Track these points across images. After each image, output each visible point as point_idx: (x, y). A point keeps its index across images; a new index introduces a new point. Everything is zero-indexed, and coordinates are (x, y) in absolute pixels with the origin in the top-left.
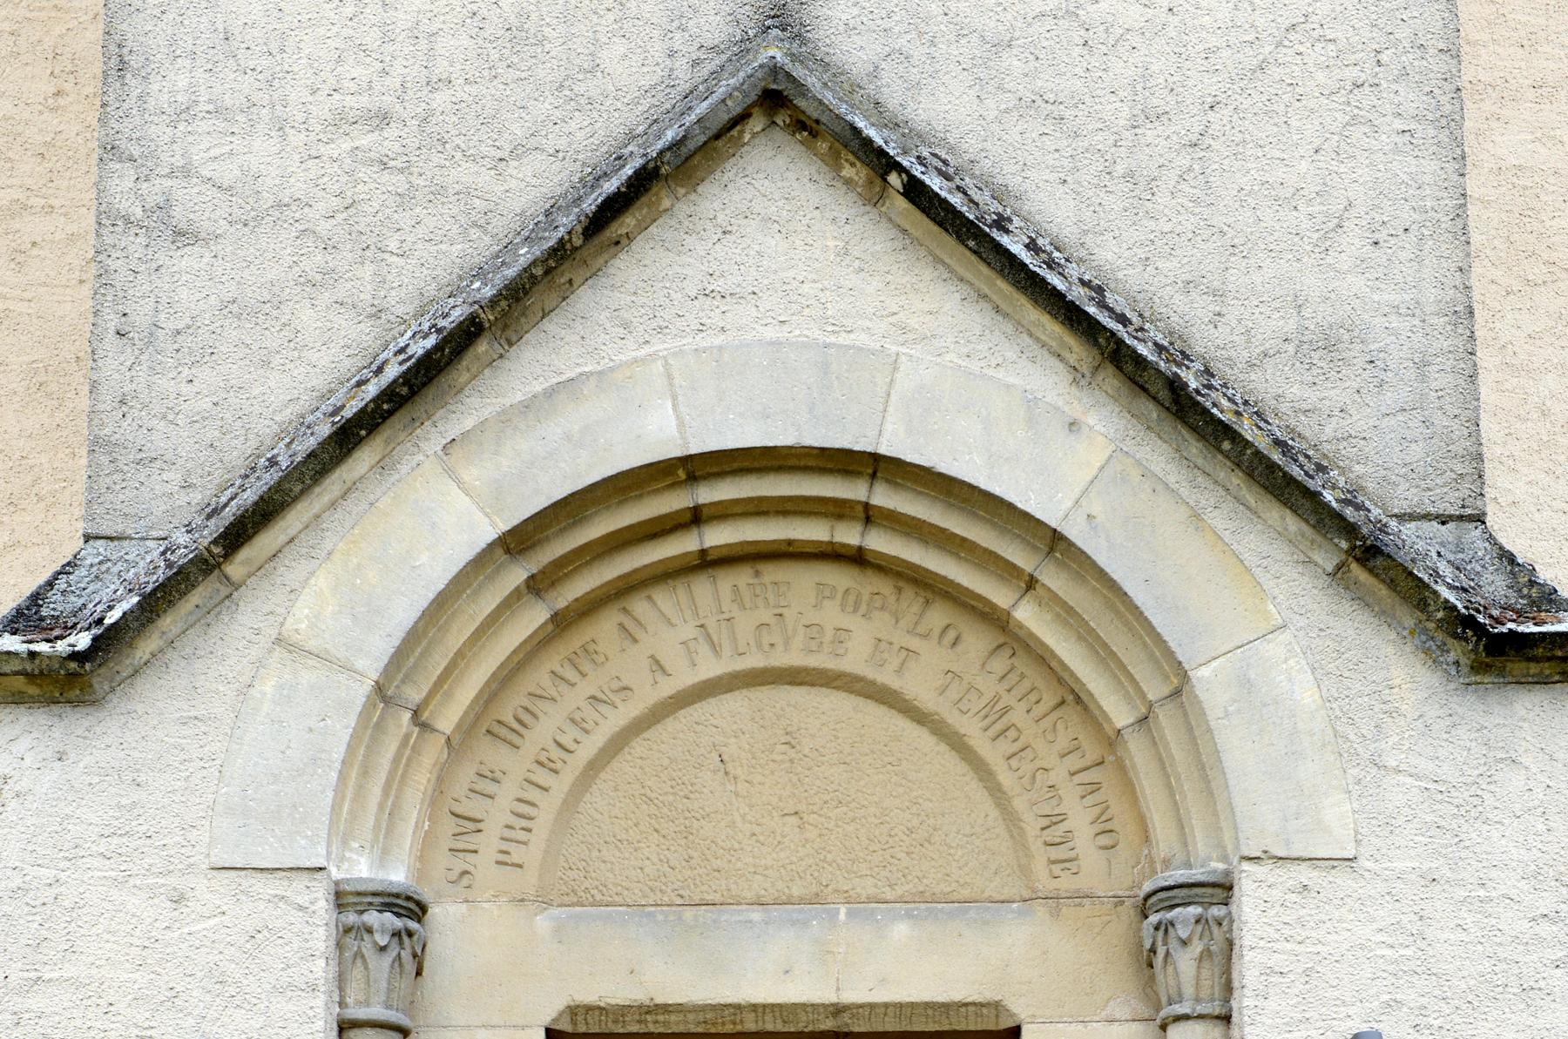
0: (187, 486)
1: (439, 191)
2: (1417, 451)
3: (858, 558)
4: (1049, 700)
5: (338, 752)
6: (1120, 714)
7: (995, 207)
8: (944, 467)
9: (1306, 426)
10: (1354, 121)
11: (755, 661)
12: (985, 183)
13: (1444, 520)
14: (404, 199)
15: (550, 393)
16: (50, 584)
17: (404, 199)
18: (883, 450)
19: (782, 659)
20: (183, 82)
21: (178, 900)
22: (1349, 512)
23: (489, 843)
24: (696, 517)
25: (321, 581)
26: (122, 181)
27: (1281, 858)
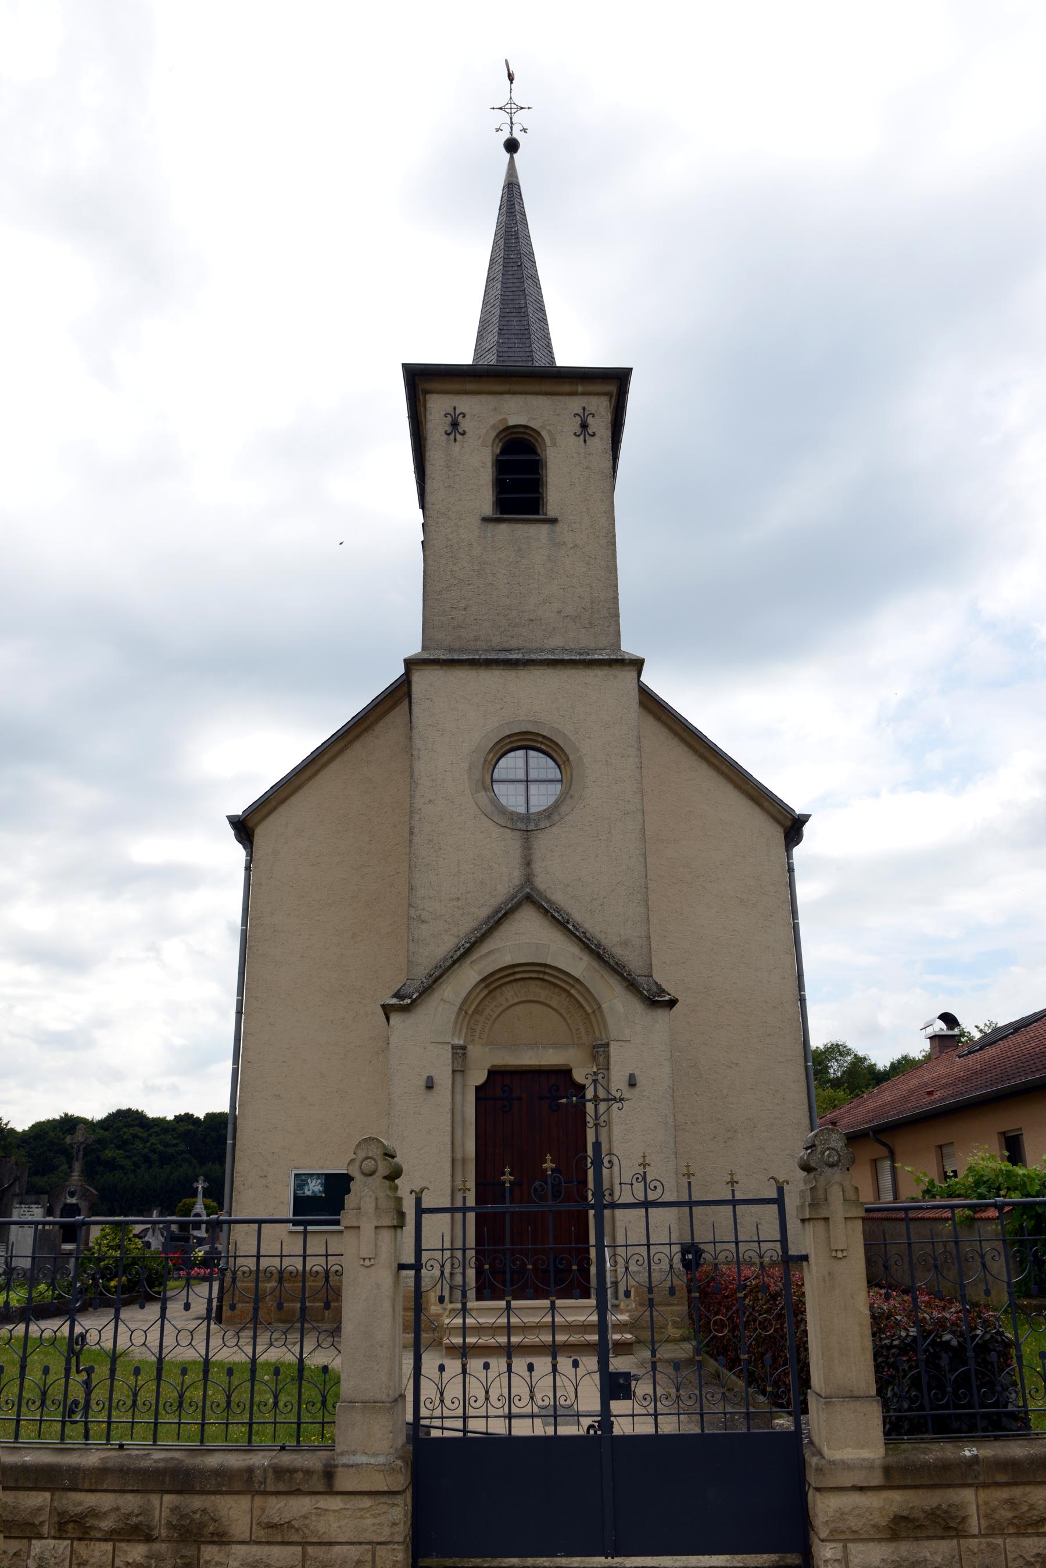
0: (425, 970)
1: (469, 913)
2: (641, 963)
3: (543, 980)
4: (577, 1007)
5: (453, 1021)
6: (589, 1011)
8: (558, 966)
9: (621, 958)
10: (630, 901)
11: (525, 999)
12: (565, 912)
13: (645, 976)
14: (462, 915)
15: (489, 952)
16: (401, 988)
17: (462, 915)
19: (528, 999)
21: (425, 1048)
22: (629, 977)
23: (477, 1034)
24: (514, 973)
25: (449, 988)
26: (413, 913)
27: (576, 1390)
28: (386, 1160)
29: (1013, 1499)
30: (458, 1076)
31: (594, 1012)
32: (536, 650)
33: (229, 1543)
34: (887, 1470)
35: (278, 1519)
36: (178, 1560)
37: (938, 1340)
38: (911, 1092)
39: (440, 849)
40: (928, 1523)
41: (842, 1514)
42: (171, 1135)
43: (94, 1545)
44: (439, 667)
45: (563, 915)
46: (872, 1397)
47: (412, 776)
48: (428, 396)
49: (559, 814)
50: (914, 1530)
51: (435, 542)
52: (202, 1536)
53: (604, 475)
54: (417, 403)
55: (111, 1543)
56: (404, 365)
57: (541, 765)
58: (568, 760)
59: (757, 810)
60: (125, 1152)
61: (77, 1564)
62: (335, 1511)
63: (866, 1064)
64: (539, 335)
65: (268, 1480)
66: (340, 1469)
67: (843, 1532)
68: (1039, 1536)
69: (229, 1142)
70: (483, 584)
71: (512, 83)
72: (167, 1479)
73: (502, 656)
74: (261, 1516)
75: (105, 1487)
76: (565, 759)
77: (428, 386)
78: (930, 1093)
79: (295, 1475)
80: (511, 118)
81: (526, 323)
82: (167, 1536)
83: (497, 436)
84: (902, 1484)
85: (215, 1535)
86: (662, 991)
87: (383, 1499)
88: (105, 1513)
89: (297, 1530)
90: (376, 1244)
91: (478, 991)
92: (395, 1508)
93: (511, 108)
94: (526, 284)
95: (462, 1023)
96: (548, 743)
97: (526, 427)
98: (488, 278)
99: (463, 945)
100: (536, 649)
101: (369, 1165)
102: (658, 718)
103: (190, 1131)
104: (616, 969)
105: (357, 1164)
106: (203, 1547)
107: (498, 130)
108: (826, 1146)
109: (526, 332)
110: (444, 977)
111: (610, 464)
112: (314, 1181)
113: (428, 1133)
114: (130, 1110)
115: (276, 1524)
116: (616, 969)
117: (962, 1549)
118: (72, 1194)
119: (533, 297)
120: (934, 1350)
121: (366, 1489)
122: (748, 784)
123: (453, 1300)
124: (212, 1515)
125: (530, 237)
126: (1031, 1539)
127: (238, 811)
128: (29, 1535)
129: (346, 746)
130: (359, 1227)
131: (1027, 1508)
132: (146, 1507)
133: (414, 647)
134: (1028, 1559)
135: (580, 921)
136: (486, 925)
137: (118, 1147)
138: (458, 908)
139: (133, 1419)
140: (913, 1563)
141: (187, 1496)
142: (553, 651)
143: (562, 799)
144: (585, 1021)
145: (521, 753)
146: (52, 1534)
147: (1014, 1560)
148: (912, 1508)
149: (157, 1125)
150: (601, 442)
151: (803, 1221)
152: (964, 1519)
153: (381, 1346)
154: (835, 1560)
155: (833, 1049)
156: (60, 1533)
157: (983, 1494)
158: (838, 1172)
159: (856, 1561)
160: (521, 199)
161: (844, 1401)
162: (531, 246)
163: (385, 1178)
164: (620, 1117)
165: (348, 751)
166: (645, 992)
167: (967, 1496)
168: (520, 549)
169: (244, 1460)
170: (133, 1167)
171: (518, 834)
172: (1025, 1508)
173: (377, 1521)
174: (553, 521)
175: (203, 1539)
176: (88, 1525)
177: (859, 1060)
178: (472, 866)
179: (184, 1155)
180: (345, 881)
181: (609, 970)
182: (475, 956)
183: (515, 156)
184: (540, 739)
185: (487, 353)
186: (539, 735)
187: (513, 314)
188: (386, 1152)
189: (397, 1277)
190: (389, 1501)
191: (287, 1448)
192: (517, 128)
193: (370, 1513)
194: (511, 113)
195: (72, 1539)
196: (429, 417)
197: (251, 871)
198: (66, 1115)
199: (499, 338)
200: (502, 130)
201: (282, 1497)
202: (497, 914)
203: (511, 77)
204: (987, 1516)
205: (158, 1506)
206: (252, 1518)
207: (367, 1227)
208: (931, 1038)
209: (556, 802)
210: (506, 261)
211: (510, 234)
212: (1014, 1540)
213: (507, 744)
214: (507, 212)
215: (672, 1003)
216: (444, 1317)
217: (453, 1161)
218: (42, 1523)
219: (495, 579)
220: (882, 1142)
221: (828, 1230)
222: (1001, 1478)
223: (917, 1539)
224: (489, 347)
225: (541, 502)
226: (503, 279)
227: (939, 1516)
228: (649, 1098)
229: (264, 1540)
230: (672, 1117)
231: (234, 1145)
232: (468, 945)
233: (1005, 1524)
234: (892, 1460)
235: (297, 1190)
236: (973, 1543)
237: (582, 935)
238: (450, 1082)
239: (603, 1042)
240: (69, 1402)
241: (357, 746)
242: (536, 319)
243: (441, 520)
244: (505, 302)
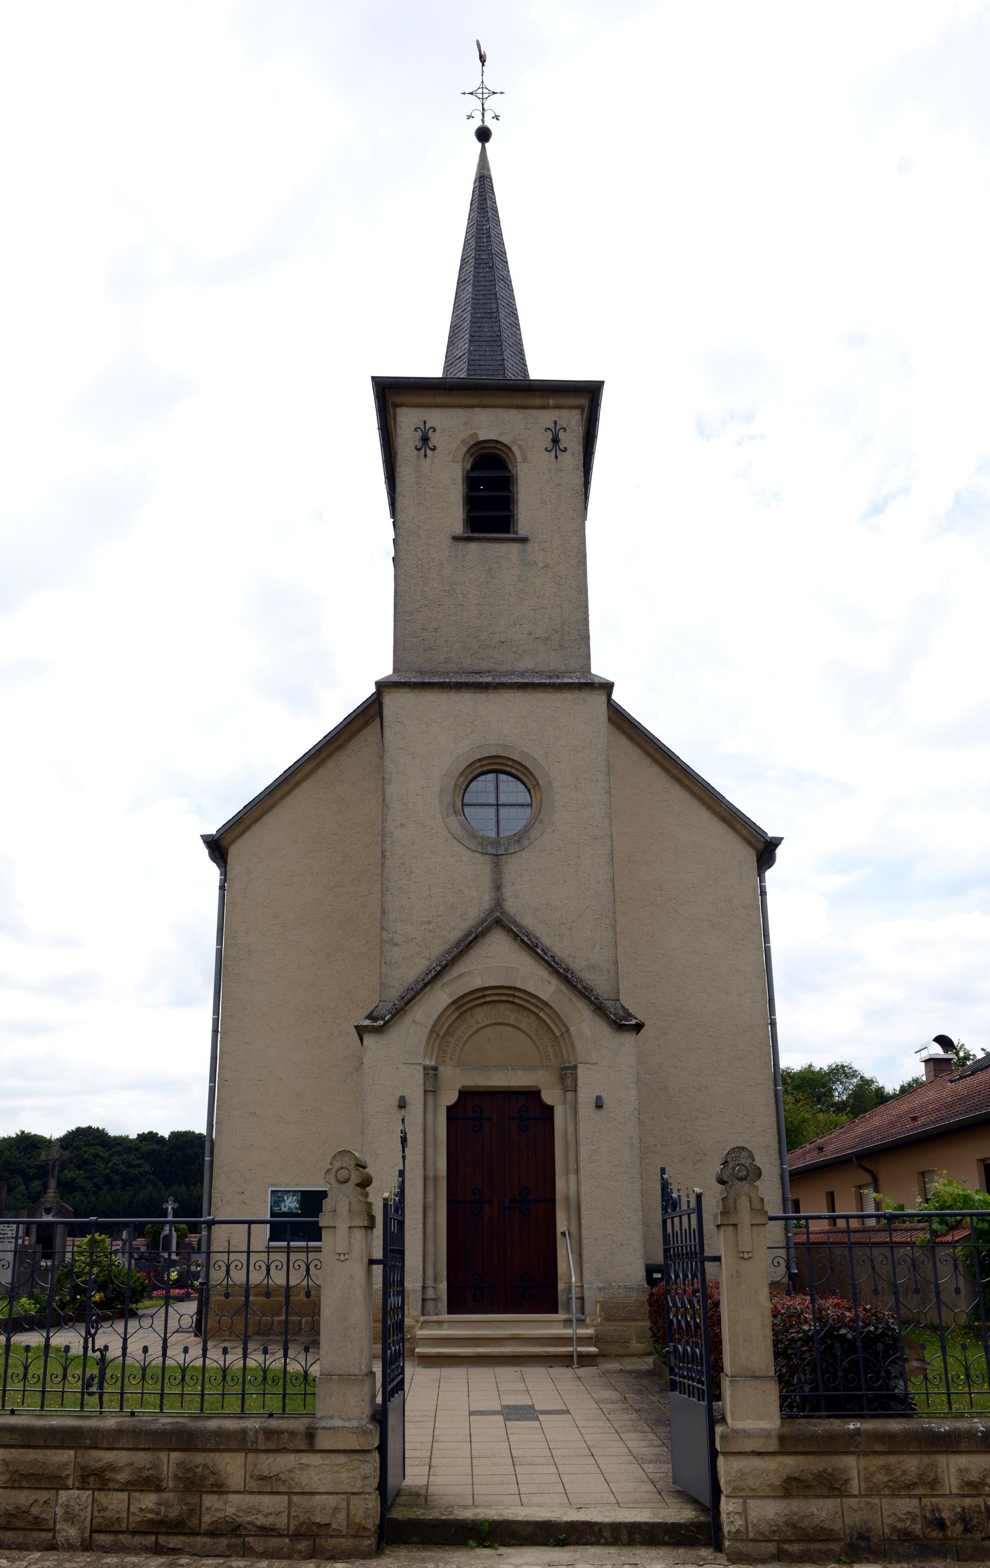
0: (397, 992)
1: (440, 936)
3: (512, 1003)
5: (424, 1043)
6: (558, 1034)
7: (536, 941)
9: (589, 982)
10: (597, 925)
14: (434, 938)
15: (459, 975)
16: (374, 1010)
18: (517, 986)
20: (395, 915)
22: (596, 1001)
24: (484, 996)
25: (421, 1010)
26: (385, 934)
28: (358, 1169)
29: (889, 1466)
30: (430, 1097)
31: (562, 1034)
32: (506, 673)
33: (227, 1493)
34: (782, 1439)
35: (268, 1472)
36: (183, 1507)
37: (836, 1333)
38: (900, 1117)
39: (412, 873)
40: (815, 1484)
41: (742, 1474)
42: (135, 1155)
43: (113, 1494)
44: (410, 690)
45: (532, 939)
46: (770, 1377)
47: (384, 800)
48: (398, 410)
49: (529, 839)
50: (804, 1490)
51: (405, 561)
52: (204, 1487)
53: (575, 492)
54: (388, 415)
55: (127, 1493)
56: (373, 378)
57: (512, 790)
58: (538, 784)
59: (730, 834)
60: (86, 1172)
61: (97, 1510)
62: (315, 1466)
63: (873, 1087)
64: (510, 341)
65: (259, 1440)
66: (320, 1431)
67: (743, 1490)
68: (910, 1498)
69: (207, 1159)
70: (454, 605)
71: (483, 65)
72: (174, 1439)
73: (472, 679)
74: (253, 1470)
75: (121, 1445)
76: (535, 783)
77: (398, 399)
78: (914, 1119)
79: (282, 1436)
80: (483, 104)
81: (498, 329)
82: (174, 1487)
83: (468, 451)
84: (794, 1450)
85: (215, 1486)
86: (629, 1015)
87: (356, 1456)
88: (121, 1468)
89: (284, 1482)
90: (349, 1242)
91: (449, 1013)
92: (366, 1464)
93: (483, 93)
94: (497, 286)
95: (434, 1045)
96: (518, 767)
97: (497, 442)
98: (459, 279)
99: (434, 968)
100: (507, 672)
101: (343, 1174)
102: (631, 738)
103: (154, 1150)
104: (584, 993)
105: (333, 1173)
106: (204, 1496)
107: (469, 117)
108: (737, 1162)
109: (498, 339)
111: (581, 481)
112: (291, 1198)
114: (90, 1128)
115: (266, 1477)
116: (584, 993)
117: (844, 1506)
118: (48, 1211)
119: (505, 301)
120: (832, 1341)
121: (342, 1448)
122: (721, 806)
124: (212, 1468)
125: (502, 235)
126: (903, 1500)
127: (212, 830)
128: (56, 1486)
129: (318, 765)
130: (335, 1227)
131: (900, 1473)
132: (156, 1462)
133: (385, 669)
134: (901, 1516)
135: (548, 945)
136: (457, 948)
137: (79, 1168)
138: (430, 931)
139: (143, 1390)
140: (802, 1517)
141: (190, 1453)
142: (522, 674)
143: (532, 823)
144: (554, 1043)
145: (491, 777)
146: (76, 1486)
147: (889, 1517)
148: (802, 1470)
149: (119, 1144)
150: (572, 459)
151: (718, 1226)
152: (847, 1481)
153: (354, 1328)
154: (737, 1513)
155: (838, 1070)
156: (83, 1483)
157: (863, 1461)
158: (747, 1185)
159: (754, 1514)
160: (493, 193)
161: (746, 1380)
162: (504, 244)
163: (357, 1185)
164: (587, 1138)
165: (321, 770)
166: (612, 1016)
167: (850, 1462)
168: (490, 569)
169: (238, 1424)
170: (94, 1189)
171: (489, 858)
172: (898, 1473)
173: (351, 1475)
174: (524, 540)
175: (205, 1490)
176: (107, 1477)
177: (866, 1083)
178: (443, 890)
179: (148, 1176)
181: (577, 993)
182: (446, 979)
183: (487, 145)
184: (510, 763)
185: (458, 361)
186: (509, 759)
187: (485, 320)
188: (358, 1163)
189: (369, 1273)
190: (362, 1459)
191: (274, 1416)
192: (488, 115)
193: (345, 1468)
194: (483, 99)
195: (93, 1490)
196: (399, 432)
197: (225, 890)
198: (23, 1132)
199: (470, 345)
200: (473, 117)
201: (271, 1455)
202: (467, 938)
203: (482, 59)
204: (866, 1479)
205: (166, 1462)
206: (245, 1472)
207: (342, 1227)
208: (926, 1061)
209: (526, 826)
210: (478, 262)
211: (481, 232)
212: (889, 1500)
213: (477, 768)
214: (478, 208)
215: (639, 1027)
216: (417, 1329)
217: (425, 1178)
218: (67, 1476)
219: (465, 600)
220: (865, 1167)
221: (736, 1234)
222: (879, 1447)
223: (806, 1497)
224: (460, 355)
225: (512, 520)
226: (474, 281)
227: (825, 1478)
229: (256, 1490)
230: (638, 1139)
231: (212, 1162)
232: (439, 968)
233: (882, 1486)
234: (786, 1430)
235: (274, 1206)
236: (854, 1502)
237: (551, 959)
238: (422, 1102)
239: (571, 1065)
240: (87, 1376)
241: (330, 764)
242: (508, 325)
243: (411, 539)
244: (476, 306)
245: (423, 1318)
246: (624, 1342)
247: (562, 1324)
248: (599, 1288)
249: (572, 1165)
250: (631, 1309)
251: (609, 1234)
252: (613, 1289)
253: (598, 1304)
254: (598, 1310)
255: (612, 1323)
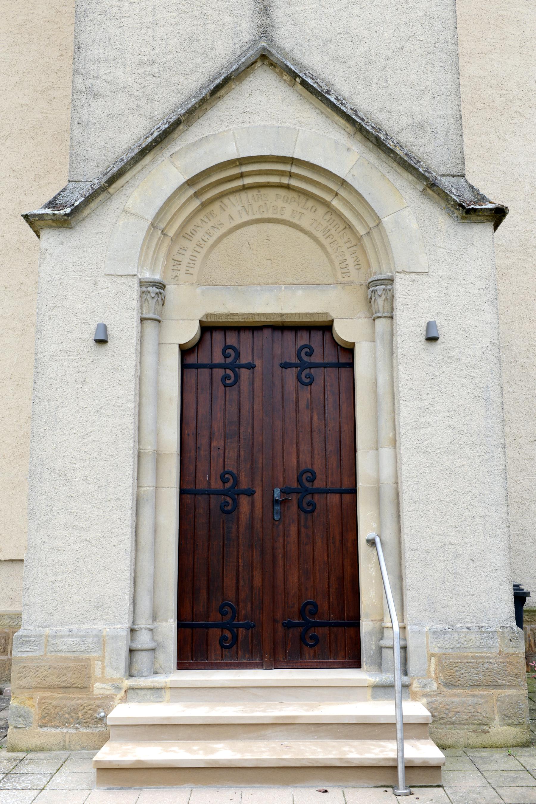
0: (98, 167)
3: (287, 187)
4: (342, 227)
6: (361, 231)
7: (326, 87)
9: (414, 150)
10: (428, 63)
11: (258, 216)
12: (323, 81)
14: (159, 85)
15: (200, 140)
16: (59, 194)
17: (159, 85)
18: (295, 156)
20: (96, 52)
21: (95, 284)
22: (426, 174)
23: (183, 268)
24: (242, 176)
25: (136, 194)
26: (79, 80)
30: (150, 327)
110: (127, 177)
113: (97, 411)
123: (134, 672)
180: (26, 108)
216: (117, 701)
228: (459, 359)
230: (498, 390)
245: (128, 683)
246: (479, 724)
247: (369, 691)
248: (434, 633)
249: (386, 434)
250: (491, 667)
251: (451, 544)
252: (459, 633)
253: (433, 659)
254: (433, 669)
255: (460, 691)
